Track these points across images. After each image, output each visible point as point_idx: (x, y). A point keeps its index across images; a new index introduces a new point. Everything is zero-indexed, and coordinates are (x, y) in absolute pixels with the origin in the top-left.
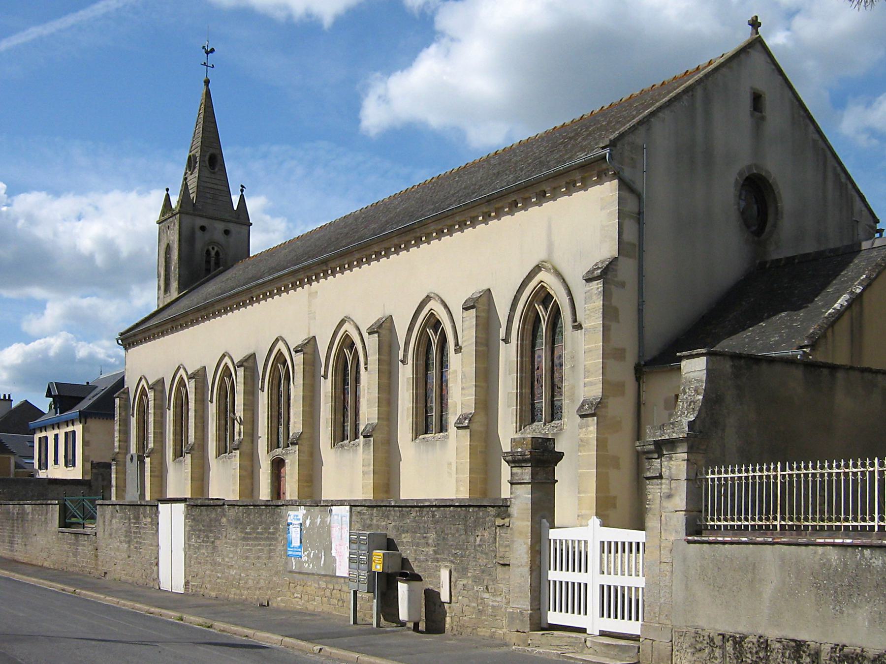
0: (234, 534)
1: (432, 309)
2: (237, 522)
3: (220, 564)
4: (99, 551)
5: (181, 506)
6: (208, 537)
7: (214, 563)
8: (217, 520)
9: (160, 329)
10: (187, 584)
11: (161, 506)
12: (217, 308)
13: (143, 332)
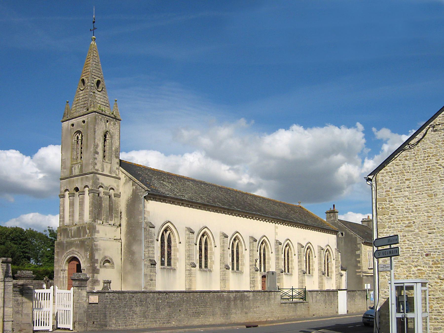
0: (359, 297)
1: (169, 222)
2: (360, 295)
3: (356, 304)
4: (310, 308)
5: (346, 291)
6: (353, 298)
7: (355, 304)
8: (355, 294)
9: (191, 204)
10: (347, 311)
11: (339, 291)
12: (235, 212)
13: (188, 202)
